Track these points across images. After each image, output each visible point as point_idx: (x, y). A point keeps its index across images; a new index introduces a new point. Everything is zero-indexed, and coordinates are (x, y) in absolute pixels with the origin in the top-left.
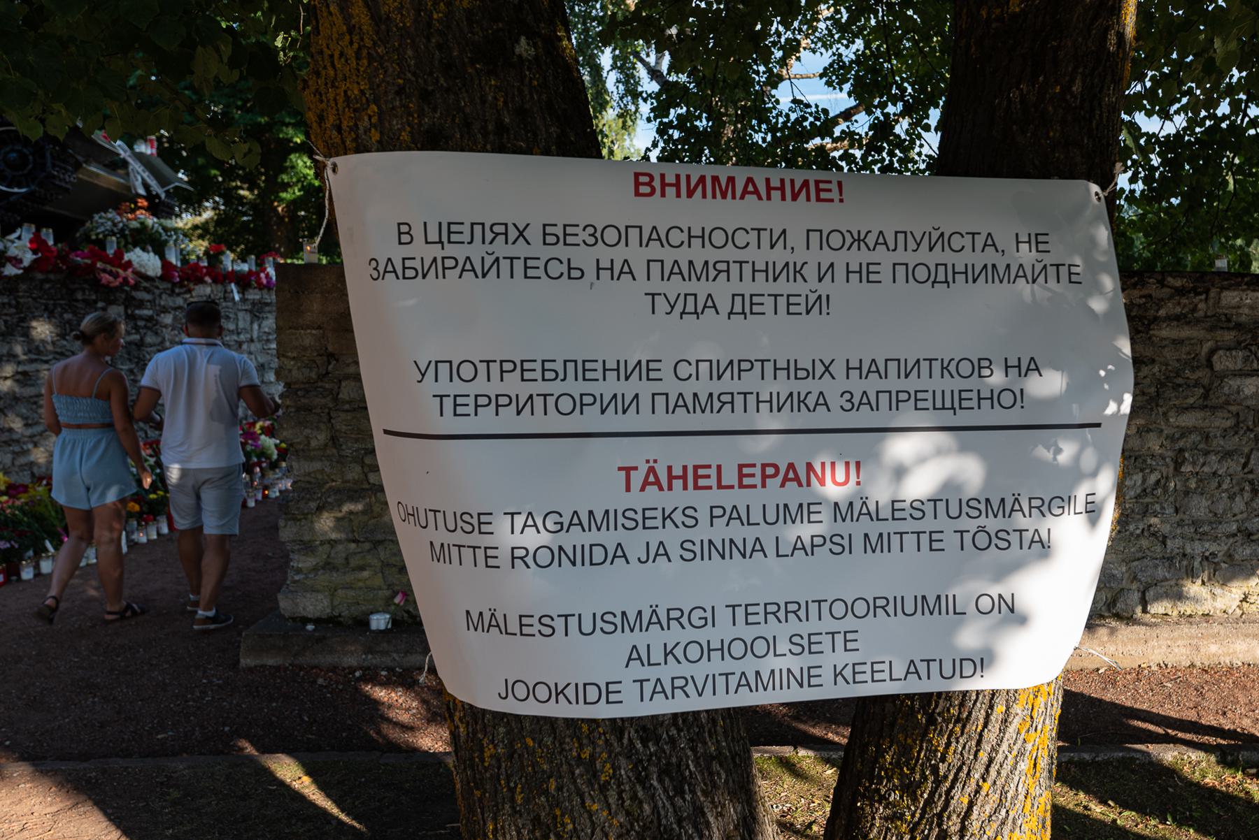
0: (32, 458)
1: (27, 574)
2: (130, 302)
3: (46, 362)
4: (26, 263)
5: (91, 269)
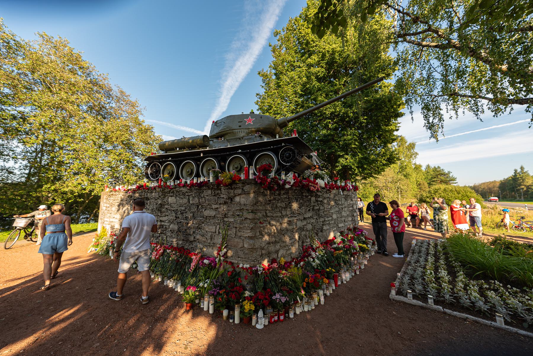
0: (291, 251)
1: (291, 316)
2: (317, 196)
3: (296, 217)
4: (292, 184)
5: (308, 185)
